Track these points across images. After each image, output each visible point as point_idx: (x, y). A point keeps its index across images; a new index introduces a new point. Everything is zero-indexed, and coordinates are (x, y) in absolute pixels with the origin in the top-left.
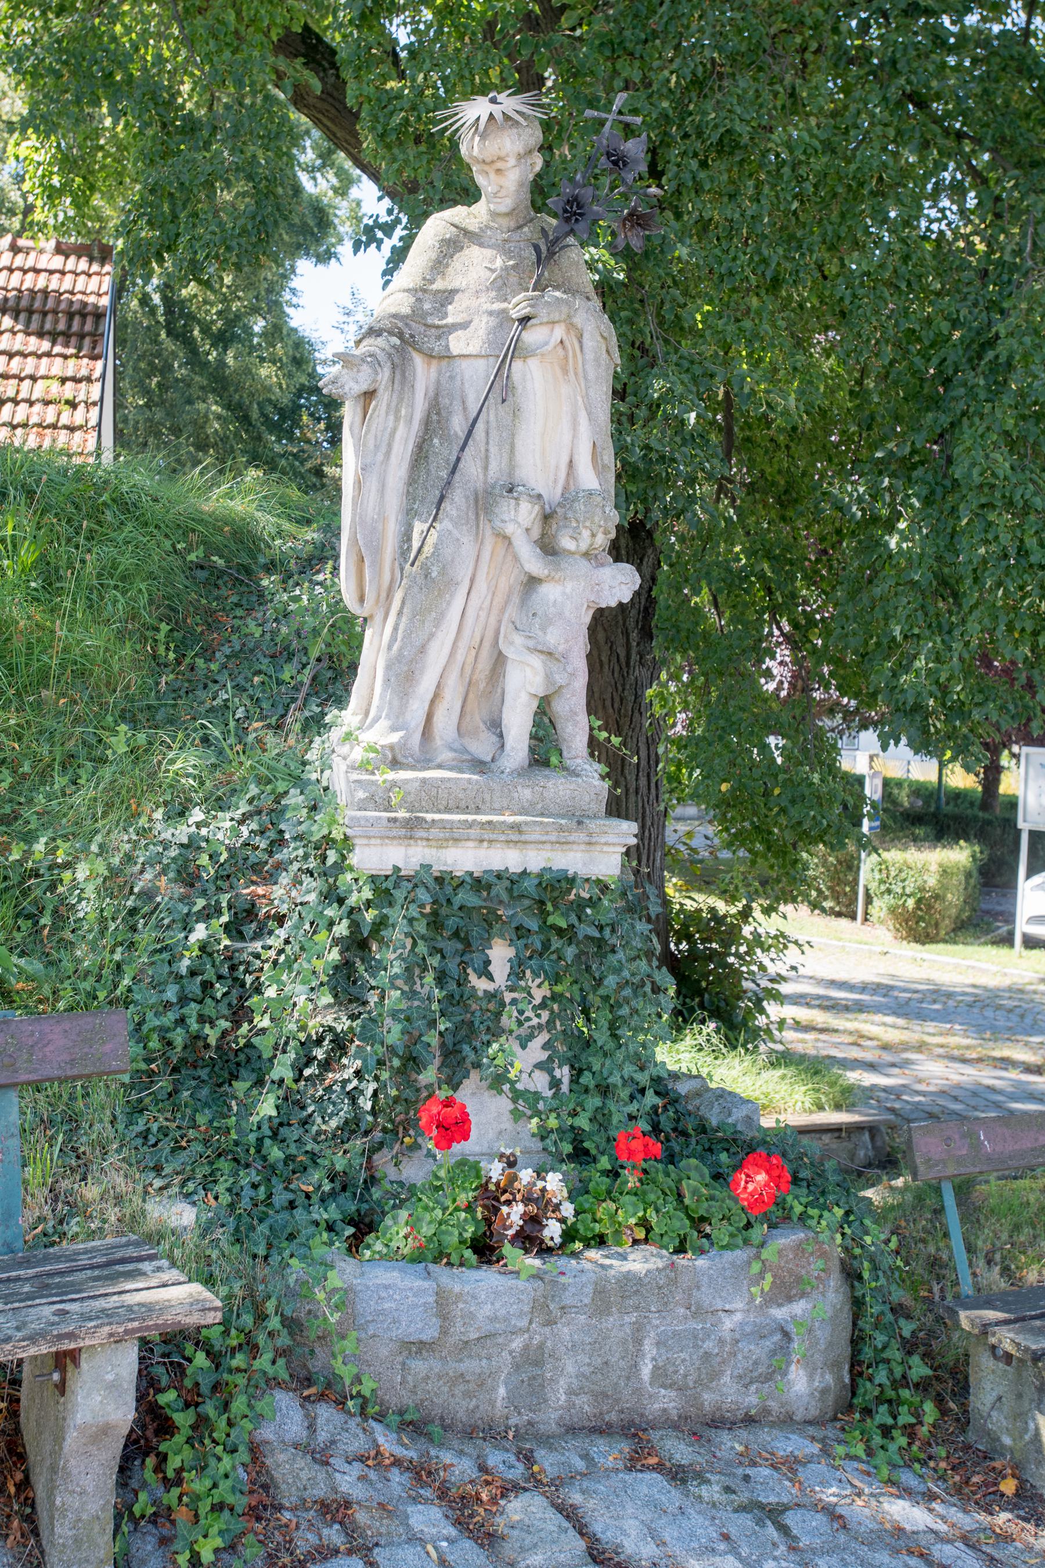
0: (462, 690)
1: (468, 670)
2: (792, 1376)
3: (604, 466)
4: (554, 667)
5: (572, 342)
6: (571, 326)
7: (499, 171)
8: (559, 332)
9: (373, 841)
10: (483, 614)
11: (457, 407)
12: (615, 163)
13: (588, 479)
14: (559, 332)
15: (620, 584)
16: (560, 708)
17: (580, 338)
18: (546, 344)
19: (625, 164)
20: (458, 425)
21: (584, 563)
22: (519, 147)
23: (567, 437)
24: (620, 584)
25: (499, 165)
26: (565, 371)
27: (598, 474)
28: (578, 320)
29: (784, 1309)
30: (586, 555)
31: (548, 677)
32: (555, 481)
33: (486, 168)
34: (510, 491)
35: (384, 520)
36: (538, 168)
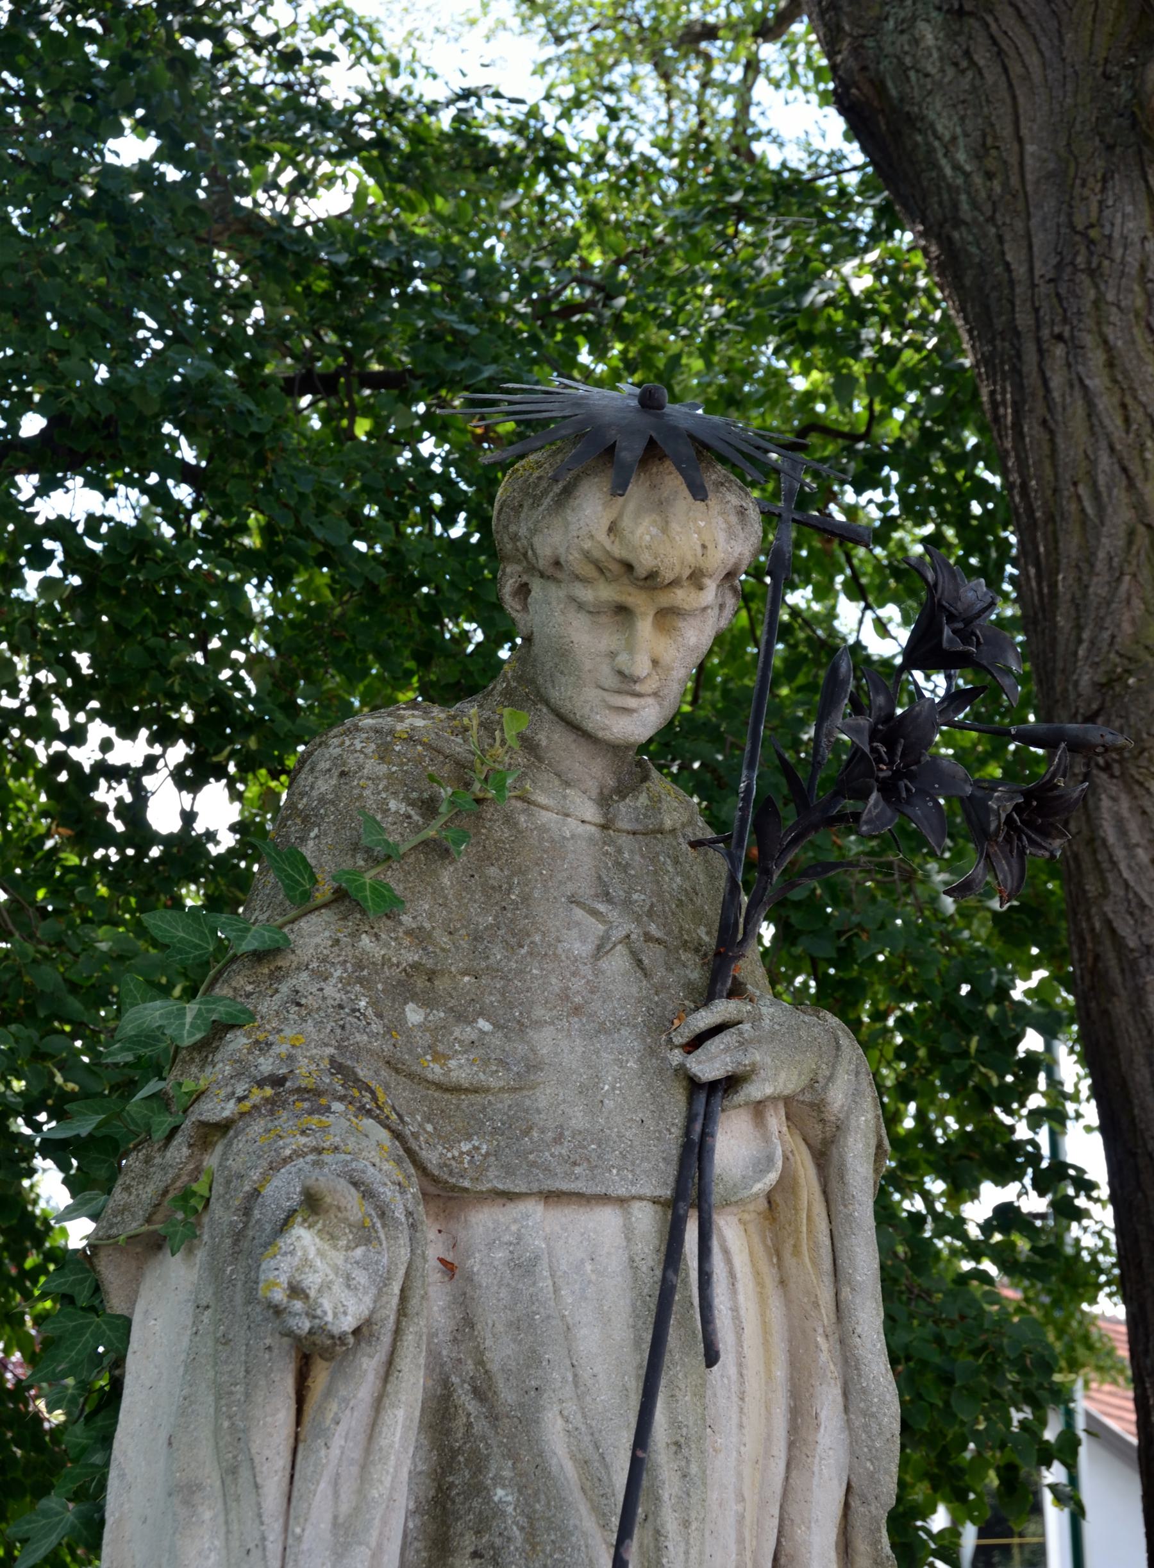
33: (636, 599)
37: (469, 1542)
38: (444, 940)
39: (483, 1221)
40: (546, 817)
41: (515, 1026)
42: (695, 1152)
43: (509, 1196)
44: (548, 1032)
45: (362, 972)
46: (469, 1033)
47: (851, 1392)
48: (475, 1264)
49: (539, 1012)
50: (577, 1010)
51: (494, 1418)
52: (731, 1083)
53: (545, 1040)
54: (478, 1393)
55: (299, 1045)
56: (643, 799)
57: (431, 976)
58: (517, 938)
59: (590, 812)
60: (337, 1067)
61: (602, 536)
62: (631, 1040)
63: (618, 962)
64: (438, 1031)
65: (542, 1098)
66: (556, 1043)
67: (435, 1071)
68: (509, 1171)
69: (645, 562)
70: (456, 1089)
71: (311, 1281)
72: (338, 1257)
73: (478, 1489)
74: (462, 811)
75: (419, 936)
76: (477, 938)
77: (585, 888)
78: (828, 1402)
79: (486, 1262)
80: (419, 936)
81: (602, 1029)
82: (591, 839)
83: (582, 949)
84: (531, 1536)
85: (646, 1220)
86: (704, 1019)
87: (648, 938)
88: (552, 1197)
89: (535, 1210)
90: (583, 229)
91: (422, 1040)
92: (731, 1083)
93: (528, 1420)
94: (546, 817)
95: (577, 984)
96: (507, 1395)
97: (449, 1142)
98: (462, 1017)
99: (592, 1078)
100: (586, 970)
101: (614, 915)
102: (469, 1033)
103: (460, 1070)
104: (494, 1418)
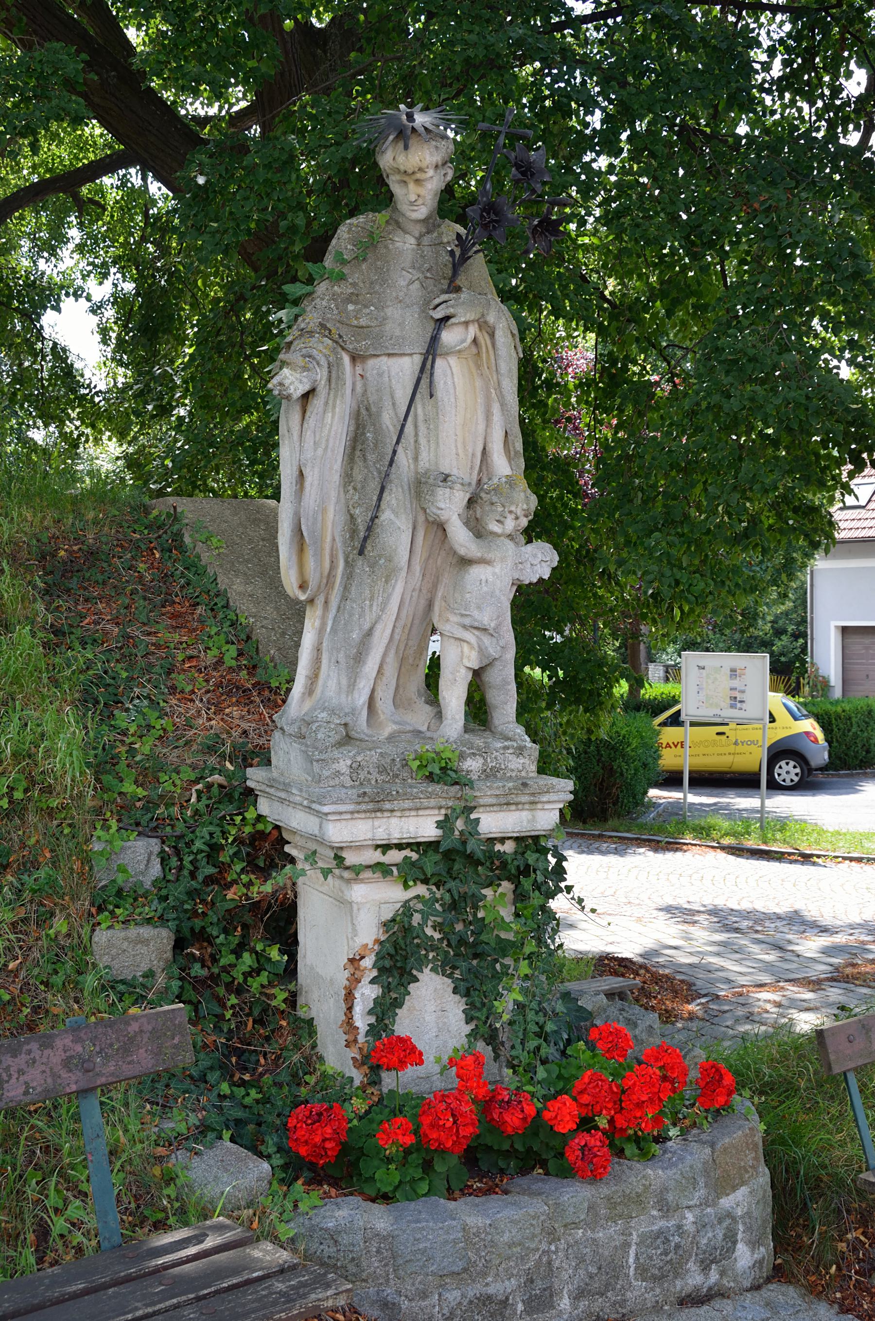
0: (397, 665)
1: (402, 647)
2: (737, 1253)
3: (516, 452)
4: (486, 640)
5: (484, 339)
6: (483, 324)
7: (417, 181)
8: (473, 330)
9: (407, 813)
10: (415, 594)
11: (387, 404)
12: (523, 174)
13: (503, 466)
14: (473, 330)
15: (540, 561)
16: (493, 677)
17: (492, 335)
18: (464, 341)
19: (533, 174)
20: (388, 421)
21: (507, 541)
22: (437, 158)
23: (481, 427)
24: (540, 561)
25: (419, 176)
26: (478, 366)
27: (509, 459)
28: (491, 319)
29: (731, 1197)
30: (510, 537)
31: (481, 650)
32: (472, 468)
33: (406, 178)
34: (445, 480)
35: (324, 511)
36: (449, 178)
37: (360, 447)
38: (361, 285)
39: (371, 362)
40: (398, 244)
41: (380, 308)
42: (434, 340)
43: (378, 356)
44: (390, 309)
45: (334, 297)
46: (368, 311)
47: (503, 405)
48: (368, 375)
49: (389, 303)
50: (400, 301)
51: (370, 415)
52: (447, 318)
53: (389, 311)
54: (367, 409)
55: (311, 319)
56: (435, 234)
57: (357, 295)
58: (385, 281)
59: (413, 241)
60: (322, 326)
61: (391, 161)
62: (416, 308)
63: (417, 285)
64: (358, 311)
65: (387, 328)
66: (393, 312)
67: (355, 322)
68: (376, 349)
69: (402, 168)
70: (362, 327)
71: (287, 382)
72: (298, 376)
73: (364, 434)
74: (370, 245)
75: (354, 285)
76: (372, 283)
77: (407, 264)
78: (496, 409)
79: (370, 374)
80: (354, 285)
81: (408, 306)
82: (413, 250)
83: (403, 283)
84: (376, 445)
85: (418, 359)
86: (437, 301)
87: (426, 278)
88: (389, 355)
89: (384, 359)
90: (71, 246)
91: (352, 314)
92: (447, 318)
93: (379, 414)
94: (398, 244)
95: (401, 294)
96: (374, 409)
97: (358, 342)
98: (366, 307)
99: (403, 321)
100: (405, 290)
101: (414, 272)
102: (368, 311)
103: (363, 322)
104: (370, 415)
